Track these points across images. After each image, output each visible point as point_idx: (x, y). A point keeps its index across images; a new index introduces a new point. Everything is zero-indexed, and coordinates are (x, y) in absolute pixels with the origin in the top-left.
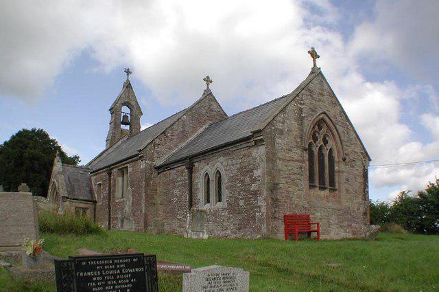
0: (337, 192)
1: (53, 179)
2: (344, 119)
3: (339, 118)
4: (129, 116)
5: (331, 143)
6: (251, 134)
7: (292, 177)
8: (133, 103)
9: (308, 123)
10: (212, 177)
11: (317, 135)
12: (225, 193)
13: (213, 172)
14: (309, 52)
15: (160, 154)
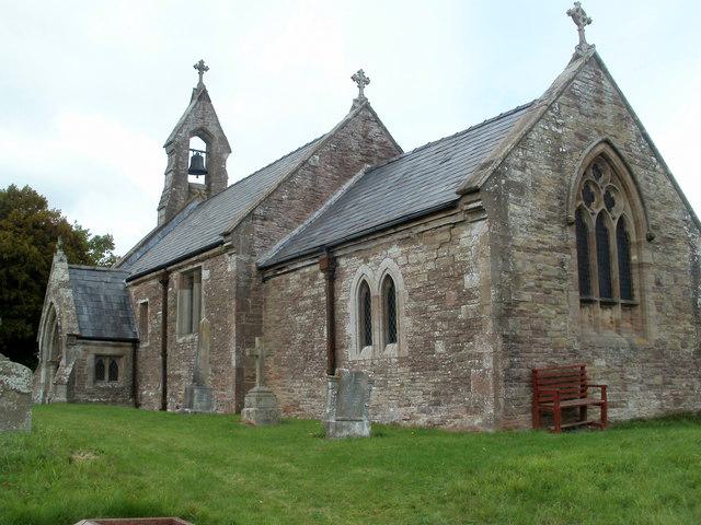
0: (638, 311)
1: (51, 299)
2: (647, 150)
3: (635, 148)
4: (204, 155)
5: (621, 203)
6: (457, 197)
7: (546, 284)
8: (212, 129)
9: (575, 166)
10: (376, 289)
11: (592, 189)
12: (404, 323)
13: (378, 279)
14: (569, 13)
15: (269, 240)
